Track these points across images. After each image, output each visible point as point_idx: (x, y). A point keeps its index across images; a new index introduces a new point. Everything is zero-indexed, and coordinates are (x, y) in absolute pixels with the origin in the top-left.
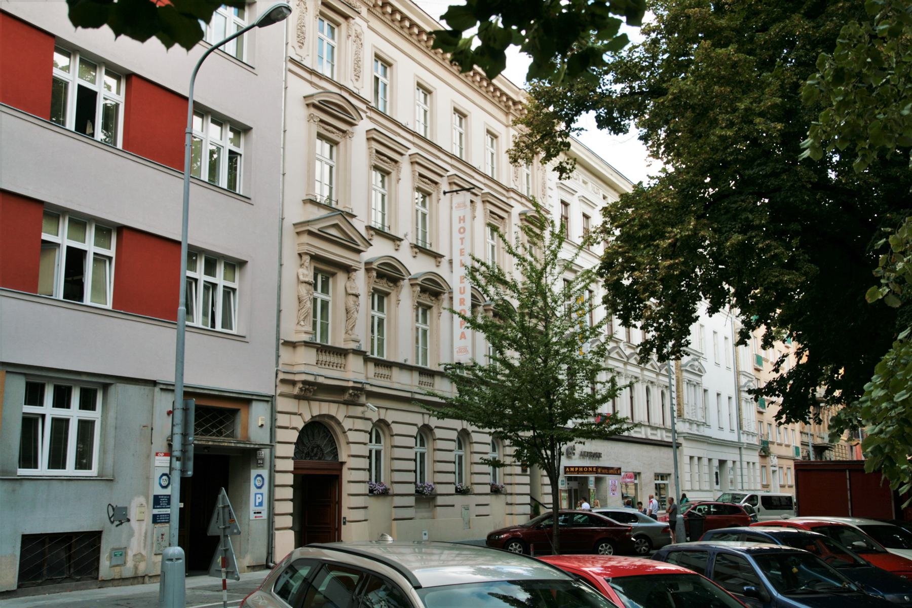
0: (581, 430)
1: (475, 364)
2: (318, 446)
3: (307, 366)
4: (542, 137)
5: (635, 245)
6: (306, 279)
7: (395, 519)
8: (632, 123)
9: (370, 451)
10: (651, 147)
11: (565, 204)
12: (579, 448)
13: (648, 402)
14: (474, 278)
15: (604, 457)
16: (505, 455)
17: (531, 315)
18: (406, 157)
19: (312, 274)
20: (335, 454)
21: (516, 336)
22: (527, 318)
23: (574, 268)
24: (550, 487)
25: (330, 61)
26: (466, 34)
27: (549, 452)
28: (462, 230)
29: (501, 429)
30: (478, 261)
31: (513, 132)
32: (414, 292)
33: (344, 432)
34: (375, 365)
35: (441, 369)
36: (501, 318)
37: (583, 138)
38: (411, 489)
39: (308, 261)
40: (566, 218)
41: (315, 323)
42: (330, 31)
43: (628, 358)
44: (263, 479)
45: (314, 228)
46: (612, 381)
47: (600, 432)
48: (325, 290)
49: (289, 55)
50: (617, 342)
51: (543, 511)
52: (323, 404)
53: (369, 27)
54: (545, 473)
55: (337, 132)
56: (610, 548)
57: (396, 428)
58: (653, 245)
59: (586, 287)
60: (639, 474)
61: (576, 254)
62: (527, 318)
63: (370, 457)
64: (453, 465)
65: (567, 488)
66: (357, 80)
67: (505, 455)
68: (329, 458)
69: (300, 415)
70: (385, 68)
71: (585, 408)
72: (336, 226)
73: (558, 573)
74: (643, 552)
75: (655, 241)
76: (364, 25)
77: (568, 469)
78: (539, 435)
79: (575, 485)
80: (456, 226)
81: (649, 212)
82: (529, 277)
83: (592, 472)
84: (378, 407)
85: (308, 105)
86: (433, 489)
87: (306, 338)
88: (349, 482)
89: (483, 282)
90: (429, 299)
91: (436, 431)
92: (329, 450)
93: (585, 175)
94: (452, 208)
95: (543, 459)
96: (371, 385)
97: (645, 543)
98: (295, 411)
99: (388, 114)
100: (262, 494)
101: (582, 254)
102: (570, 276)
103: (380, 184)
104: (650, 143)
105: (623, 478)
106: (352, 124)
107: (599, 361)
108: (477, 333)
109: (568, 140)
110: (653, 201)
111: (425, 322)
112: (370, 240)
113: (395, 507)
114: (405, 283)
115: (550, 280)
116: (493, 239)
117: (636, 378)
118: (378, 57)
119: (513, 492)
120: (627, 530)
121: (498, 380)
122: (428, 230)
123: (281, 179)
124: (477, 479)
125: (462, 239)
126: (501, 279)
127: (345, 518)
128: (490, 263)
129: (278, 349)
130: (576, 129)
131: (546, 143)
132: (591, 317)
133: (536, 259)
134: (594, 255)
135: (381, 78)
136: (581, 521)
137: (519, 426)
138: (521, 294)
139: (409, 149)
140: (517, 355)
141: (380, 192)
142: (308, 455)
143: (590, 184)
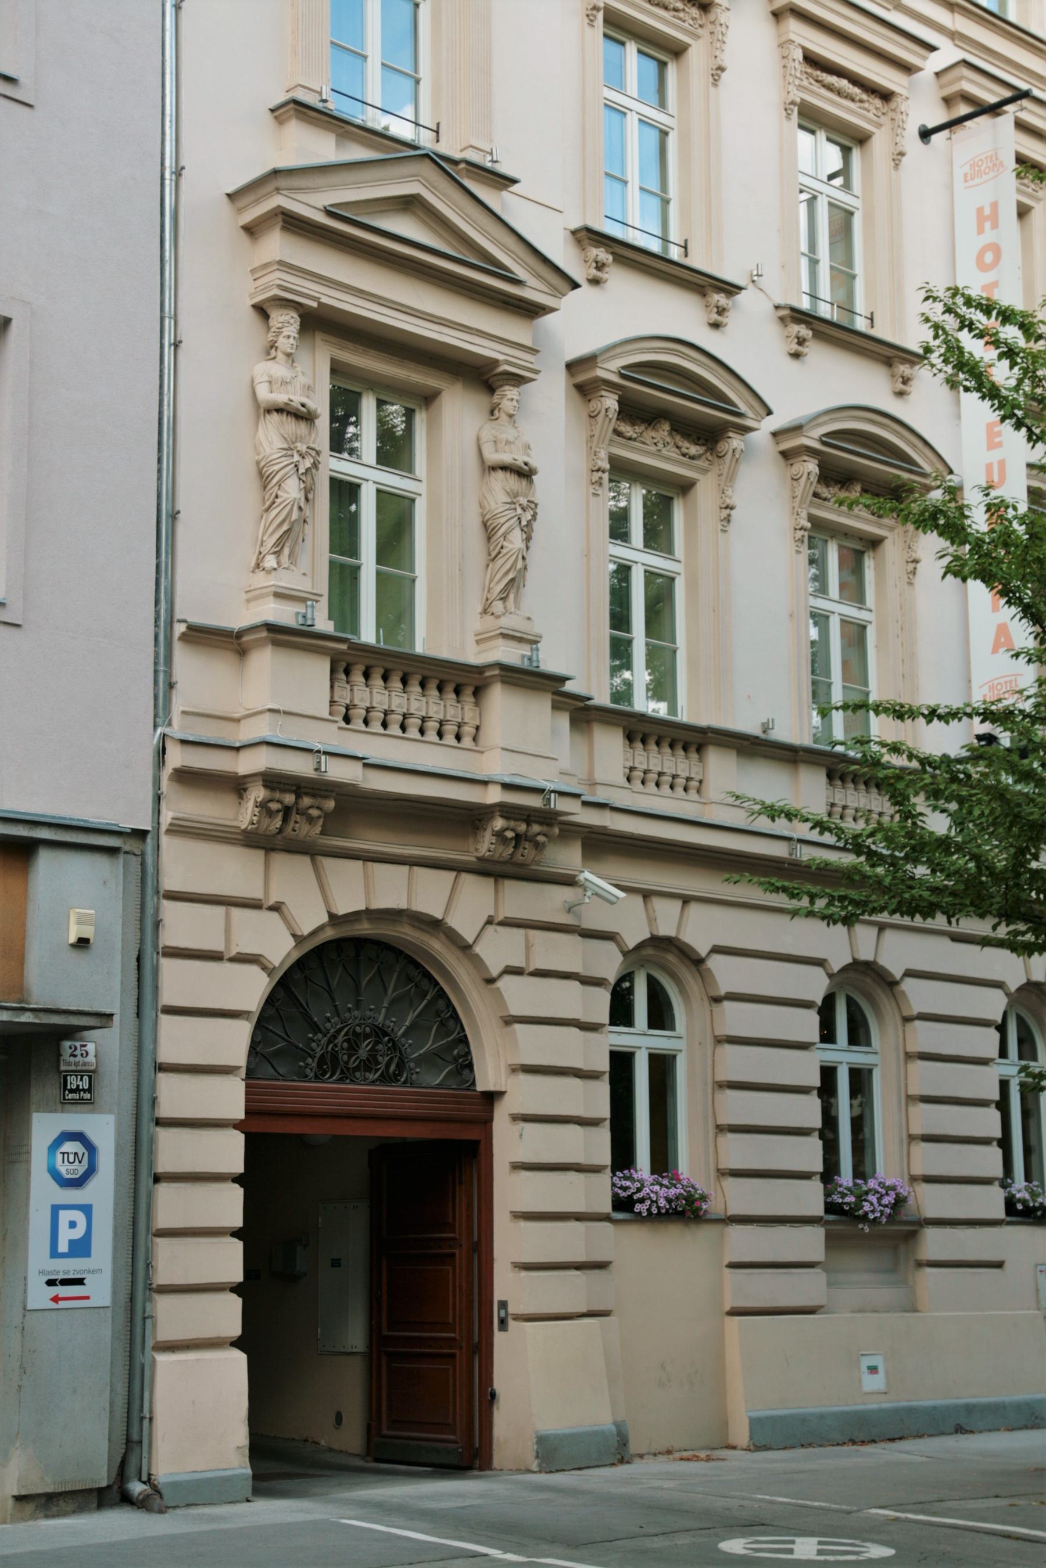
2: (380, 1032)
3: (281, 719)
20: (466, 1065)
28: (989, 257)
32: (795, 479)
44: (91, 1148)
69: (276, 908)
72: (409, 204)
88: (519, 1167)
98: (255, 892)
100: (87, 1210)
127: (503, 1305)
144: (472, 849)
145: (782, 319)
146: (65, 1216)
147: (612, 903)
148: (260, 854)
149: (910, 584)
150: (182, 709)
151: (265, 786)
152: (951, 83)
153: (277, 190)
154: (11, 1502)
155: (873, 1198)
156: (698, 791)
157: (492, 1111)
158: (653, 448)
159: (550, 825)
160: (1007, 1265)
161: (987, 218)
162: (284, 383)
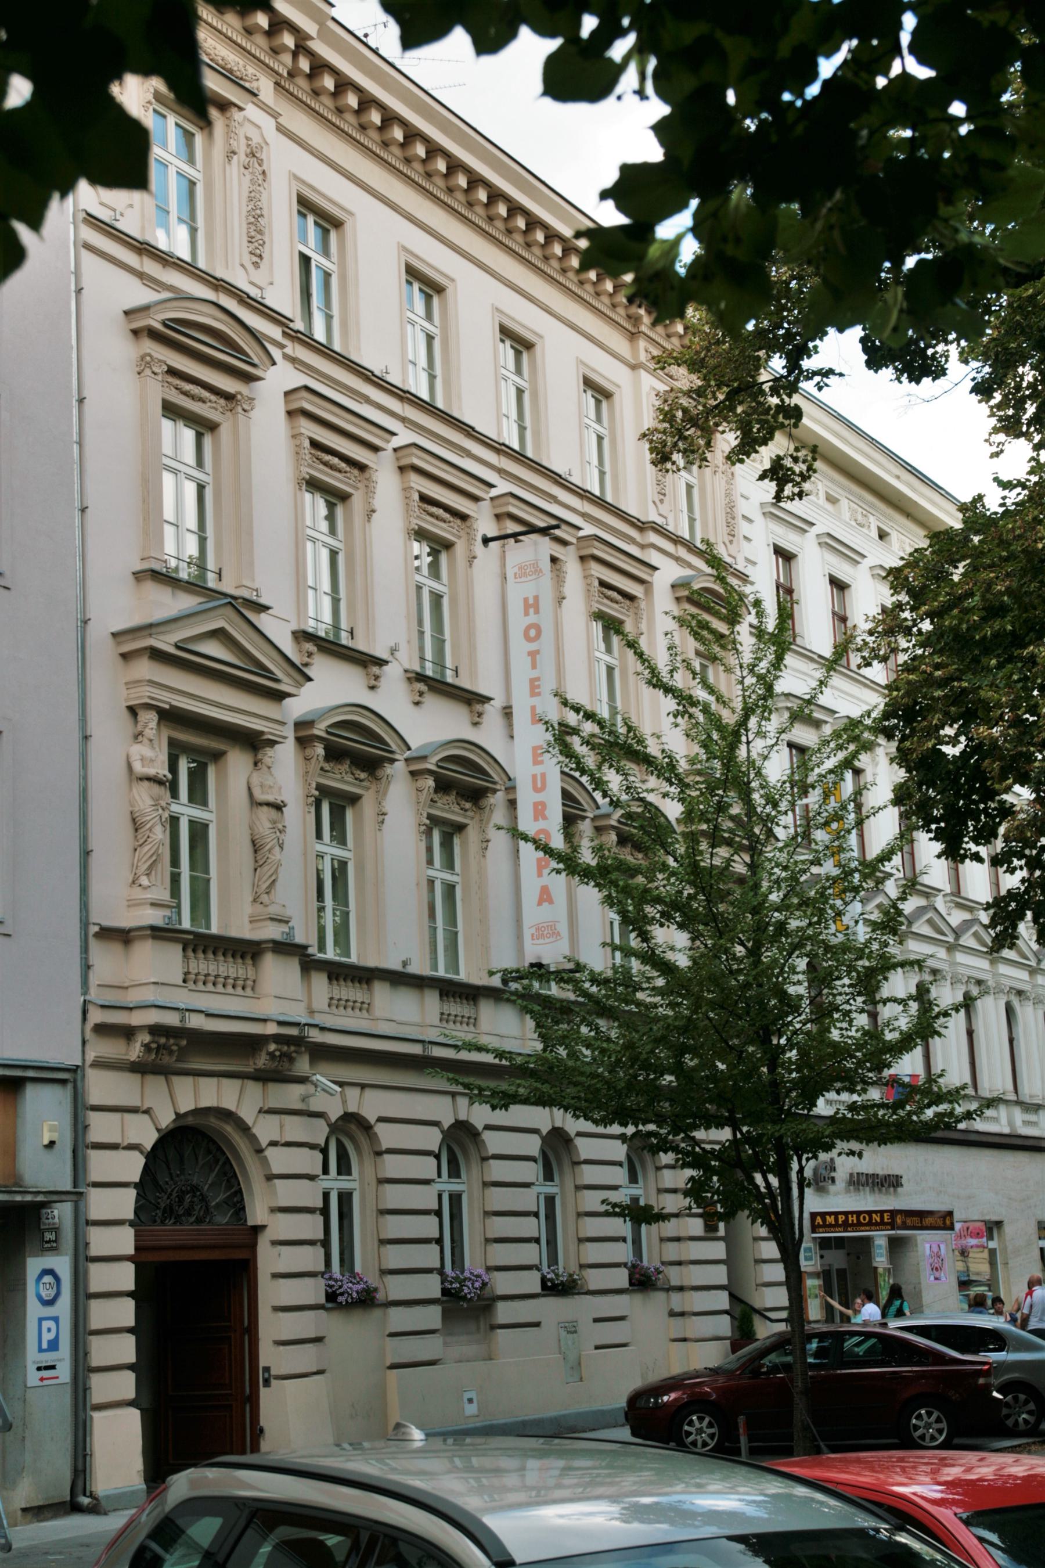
0: (852, 1120)
1: (579, 968)
2: (194, 1189)
4: (729, 396)
5: (976, 660)
6: (151, 771)
7: (394, 1366)
8: (953, 350)
9: (326, 1196)
10: (999, 406)
11: (784, 555)
12: (845, 1166)
13: (1011, 1041)
14: (567, 752)
15: (908, 1185)
16: (660, 1191)
17: (715, 839)
18: (387, 456)
19: (163, 757)
20: (237, 1205)
21: (680, 892)
22: (704, 846)
23: (818, 715)
24: (780, 1267)
25: (186, 216)
26: (666, 230)
27: (774, 1181)
28: (532, 633)
29: (652, 1127)
30: (577, 709)
31: (652, 385)
33: (260, 1151)
34: (330, 978)
35: (496, 981)
36: (638, 847)
37: (834, 394)
38: (432, 1286)
39: (153, 724)
40: (790, 591)
41: (175, 879)
42: (182, 141)
43: (957, 933)
45: (165, 643)
46: (922, 993)
47: (900, 1124)
48: (198, 794)
49: (82, 206)
50: (927, 895)
51: (765, 1331)
52: (203, 1081)
53: (281, 129)
54: (763, 1231)
55: (213, 398)
56: (938, 1420)
57: (388, 1136)
58: (1020, 658)
59: (847, 763)
60: (999, 1224)
61: (821, 682)
62: (704, 846)
63: (325, 1211)
64: (533, 1220)
65: (819, 1269)
66: (256, 265)
67: (660, 1191)
68: (223, 1219)
69: (147, 1112)
70: (326, 232)
71: (860, 1064)
72: (219, 634)
73: (833, 1502)
74: (1022, 1426)
75: (1025, 647)
76: (268, 124)
77: (819, 1220)
78: (747, 1139)
79: (838, 1259)
80: (518, 622)
81: (1008, 575)
82: (704, 745)
83: (881, 1225)
84: (341, 1084)
85: (135, 332)
86: (484, 1284)
87: (155, 917)
88: (276, 1276)
89: (591, 760)
90: (456, 808)
91: (488, 1136)
92: (222, 1197)
93: (832, 481)
94: (505, 578)
95: (760, 1197)
96: (323, 1029)
97: (1026, 1402)
98: (136, 1102)
99: (337, 347)
100: (56, 1319)
101: (836, 680)
102: (804, 735)
103: (324, 526)
104: (998, 397)
105: (960, 1236)
106: (249, 378)
107: (887, 945)
108: (583, 887)
109: (796, 400)
110: (1017, 547)
111: (449, 864)
112: (306, 665)
113: (392, 1335)
114: (398, 770)
115: (759, 745)
116: (609, 650)
117: (979, 982)
118: (305, 205)
119: (686, 1283)
120: (980, 1373)
121: (639, 1004)
122: (447, 635)
123: (77, 521)
124: (594, 1253)
125: (533, 654)
126: (637, 752)
127: (267, 1369)
128: (604, 713)
129: (85, 949)
130: (815, 373)
131: (739, 410)
132: (861, 836)
133: (719, 699)
134: (871, 685)
135: (317, 258)
136: (860, 1350)
137: (694, 1116)
138: (688, 786)
139: (394, 434)
140: (681, 939)
141: (325, 545)
142: (169, 1212)
143: (844, 503)
144: (251, 1063)
145: (409, 679)
146: (46, 1324)
147: (332, 1095)
148: (139, 1076)
149: (484, 856)
150: (97, 983)
151: (150, 1033)
152: (501, 506)
153: (150, 635)
154: (19, 1513)
155: (469, 1284)
156: (253, 989)
157: (256, 1239)
158: (339, 776)
159: (299, 1045)
160: (542, 1324)
161: (531, 606)
162: (152, 761)
